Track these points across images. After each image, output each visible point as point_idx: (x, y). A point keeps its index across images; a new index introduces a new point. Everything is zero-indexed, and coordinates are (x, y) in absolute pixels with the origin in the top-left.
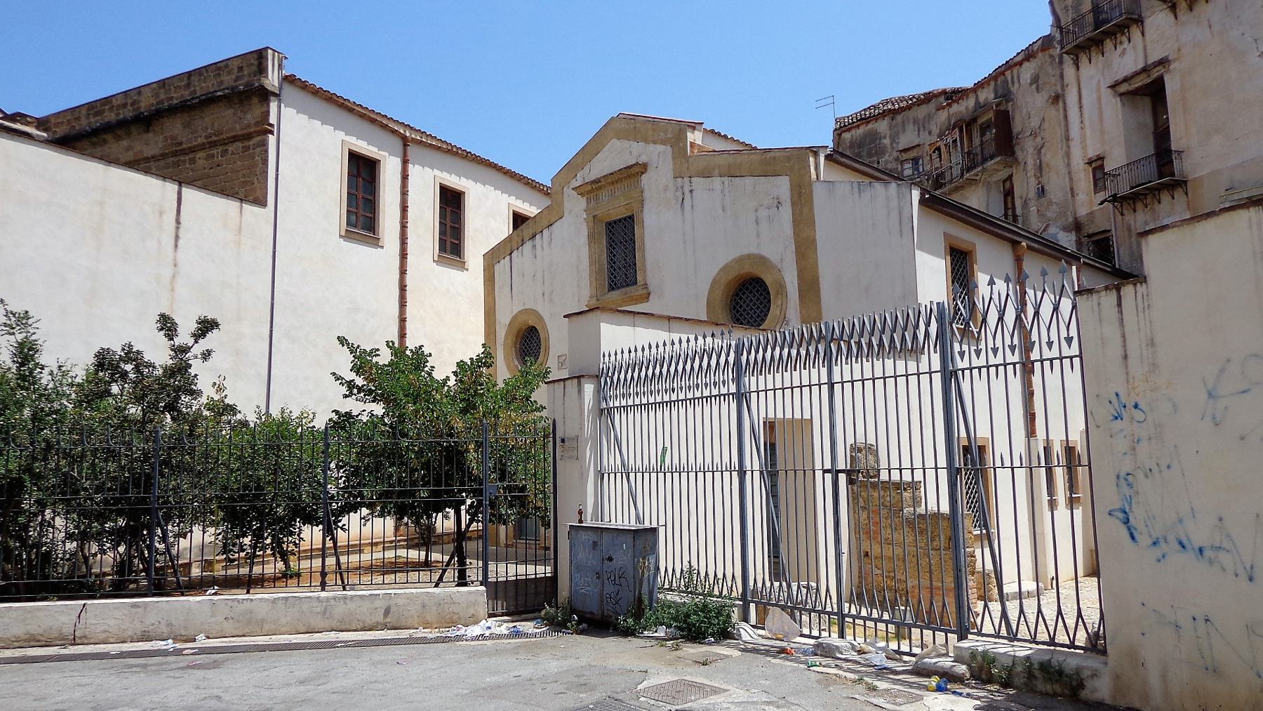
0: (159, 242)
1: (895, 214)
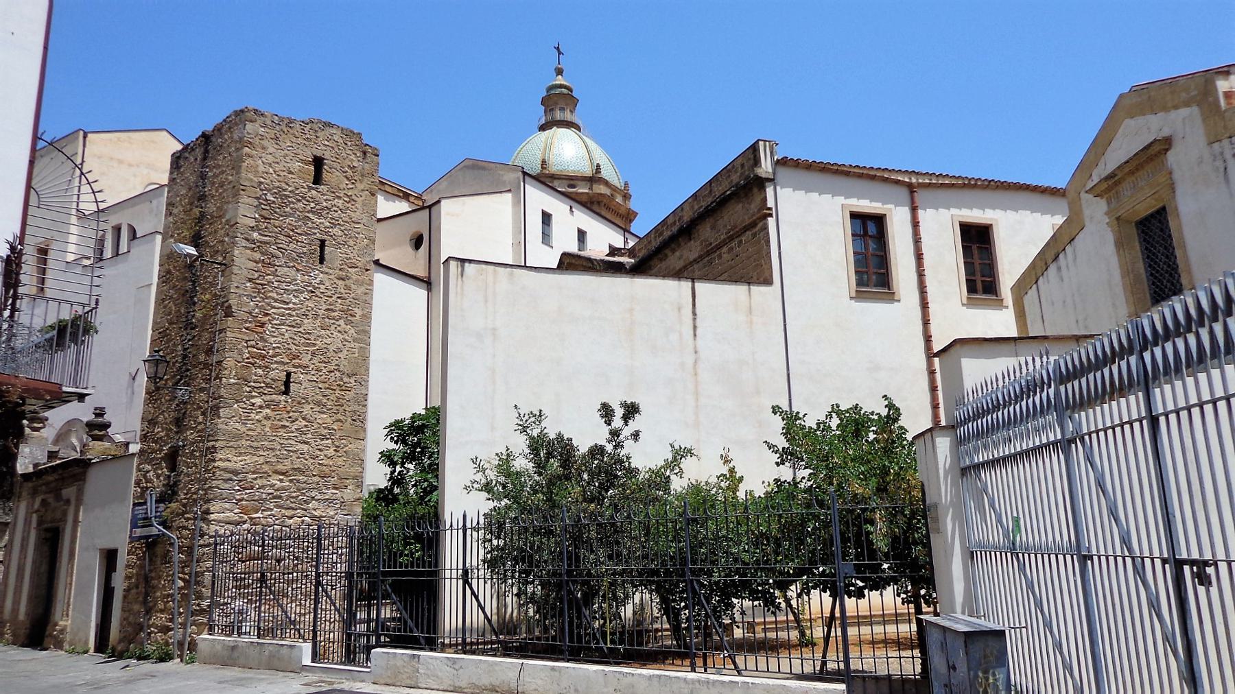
0: (681, 335)
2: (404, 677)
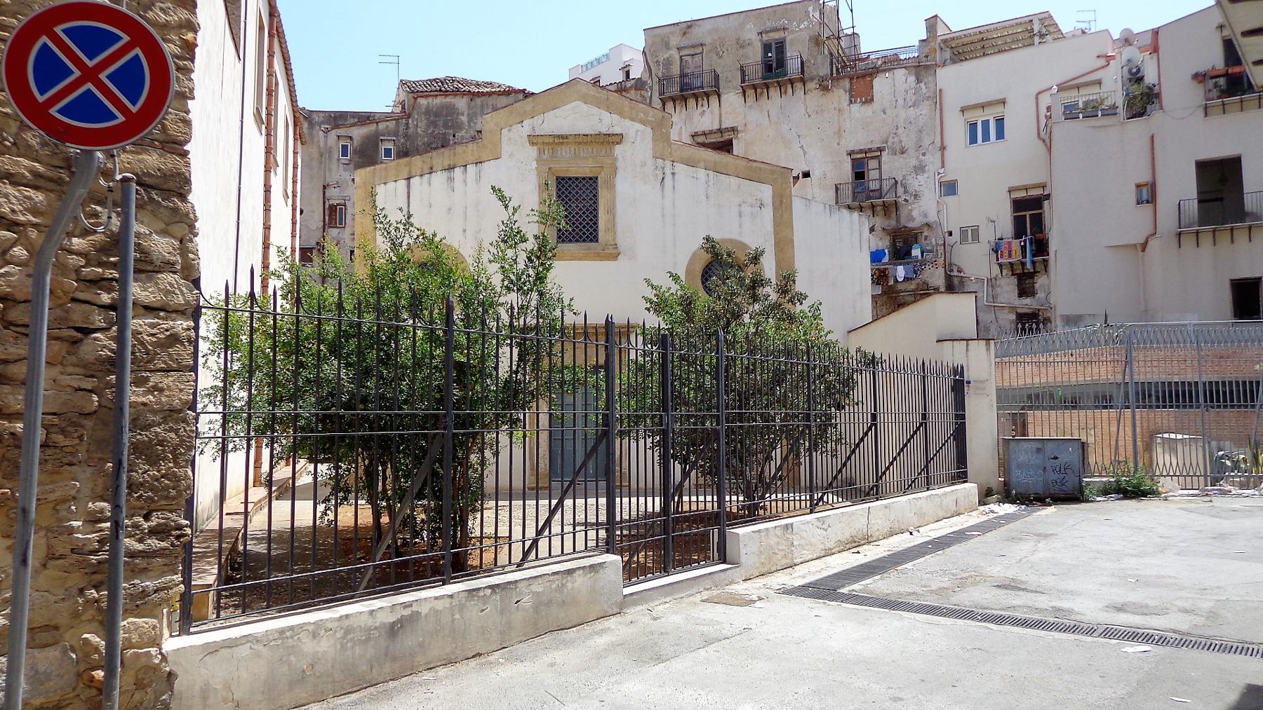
1: (857, 235)
2: (779, 557)
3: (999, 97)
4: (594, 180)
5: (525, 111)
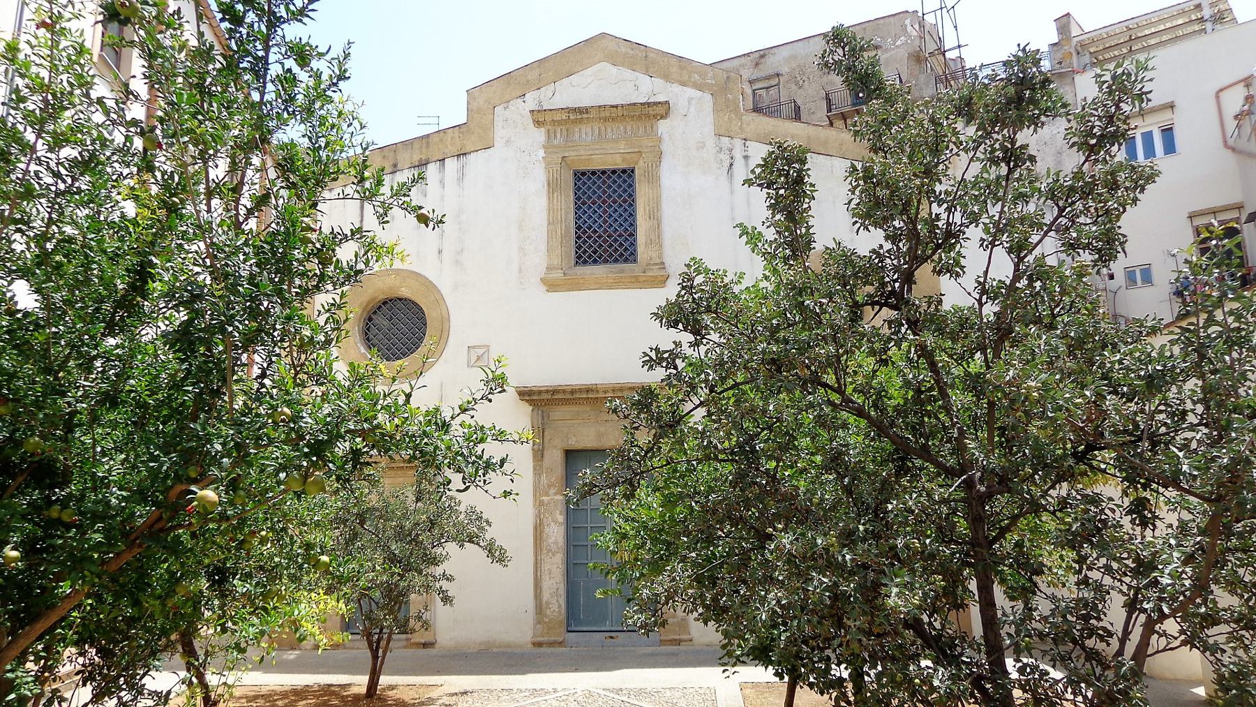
3: (1168, 100)
4: (628, 173)
5: (528, 81)
